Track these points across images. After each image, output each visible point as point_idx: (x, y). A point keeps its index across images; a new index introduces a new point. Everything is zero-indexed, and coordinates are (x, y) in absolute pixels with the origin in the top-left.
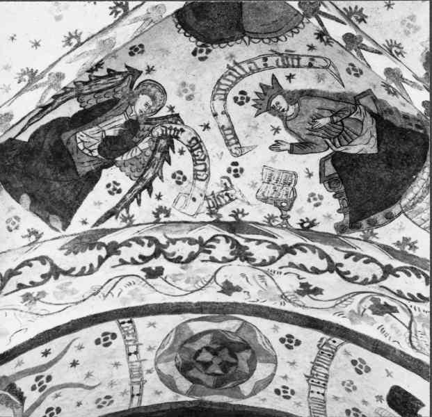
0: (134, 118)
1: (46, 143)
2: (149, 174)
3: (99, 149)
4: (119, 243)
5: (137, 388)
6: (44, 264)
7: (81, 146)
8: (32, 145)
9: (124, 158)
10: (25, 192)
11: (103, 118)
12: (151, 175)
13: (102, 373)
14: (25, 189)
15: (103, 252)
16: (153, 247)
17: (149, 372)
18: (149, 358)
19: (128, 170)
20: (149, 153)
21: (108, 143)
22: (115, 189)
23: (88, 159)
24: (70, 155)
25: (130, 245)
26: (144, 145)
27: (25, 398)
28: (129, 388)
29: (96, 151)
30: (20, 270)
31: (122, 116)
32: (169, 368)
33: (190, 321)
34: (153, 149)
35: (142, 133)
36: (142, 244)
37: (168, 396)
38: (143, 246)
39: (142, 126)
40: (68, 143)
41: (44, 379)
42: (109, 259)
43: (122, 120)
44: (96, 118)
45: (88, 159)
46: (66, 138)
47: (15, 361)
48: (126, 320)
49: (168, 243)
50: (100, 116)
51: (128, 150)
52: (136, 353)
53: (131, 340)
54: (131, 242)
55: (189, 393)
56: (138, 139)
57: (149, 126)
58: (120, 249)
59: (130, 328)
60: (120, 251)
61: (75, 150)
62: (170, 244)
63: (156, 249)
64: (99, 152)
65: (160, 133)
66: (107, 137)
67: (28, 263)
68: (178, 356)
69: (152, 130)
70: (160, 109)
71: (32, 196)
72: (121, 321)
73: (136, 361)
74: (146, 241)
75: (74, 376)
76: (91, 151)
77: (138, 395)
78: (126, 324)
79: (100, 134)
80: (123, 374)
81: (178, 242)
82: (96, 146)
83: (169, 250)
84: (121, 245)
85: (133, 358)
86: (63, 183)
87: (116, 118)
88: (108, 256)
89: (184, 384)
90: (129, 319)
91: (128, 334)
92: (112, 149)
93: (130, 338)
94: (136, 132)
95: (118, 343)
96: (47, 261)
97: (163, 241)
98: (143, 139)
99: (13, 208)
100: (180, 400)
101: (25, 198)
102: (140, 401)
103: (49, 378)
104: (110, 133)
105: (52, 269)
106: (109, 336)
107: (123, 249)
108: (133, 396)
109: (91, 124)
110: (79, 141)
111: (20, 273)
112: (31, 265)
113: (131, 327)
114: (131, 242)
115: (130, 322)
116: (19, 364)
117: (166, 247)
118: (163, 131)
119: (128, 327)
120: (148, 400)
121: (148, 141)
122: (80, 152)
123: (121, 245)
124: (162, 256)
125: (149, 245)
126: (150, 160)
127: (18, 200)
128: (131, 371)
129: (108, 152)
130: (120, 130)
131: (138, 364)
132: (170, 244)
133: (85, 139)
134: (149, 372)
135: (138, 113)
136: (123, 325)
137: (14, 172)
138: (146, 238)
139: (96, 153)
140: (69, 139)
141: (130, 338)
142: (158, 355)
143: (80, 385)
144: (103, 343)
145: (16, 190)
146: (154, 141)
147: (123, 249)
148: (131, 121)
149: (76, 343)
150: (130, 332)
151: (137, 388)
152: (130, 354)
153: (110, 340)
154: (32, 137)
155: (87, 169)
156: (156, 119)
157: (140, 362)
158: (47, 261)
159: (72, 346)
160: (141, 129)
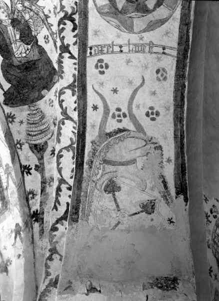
0: (10, 21)
1: (17, 75)
2: (41, 14)
3: (27, 44)
4: (61, 44)
5: (155, 49)
6: (64, 93)
7: (24, 55)
8: (15, 83)
9: (33, 30)
10: (41, 91)
11: (8, 40)
12: (43, 14)
13: (134, 74)
14: (39, 91)
15: (67, 55)
16: (66, 21)
17: (141, 39)
18: (125, 37)
19: (39, 29)
20: (32, 13)
21: (23, 39)
22: (152, 114)
23: (32, 52)
24: (28, 62)
25: (63, 37)
26: (27, 17)
27: (124, 128)
28: (154, 55)
29: (28, 46)
30: (64, 107)
31: (8, 28)
32: (139, 23)
33: (96, 5)
34: (30, 11)
35: (20, 17)
36: (63, 29)
37: (174, 25)
38: (65, 29)
39: (15, 17)
40: (20, 62)
41: (117, 113)
42: (71, 52)
43: (10, 29)
44: (6, 44)
45: (32, 52)
46: (18, 63)
47: (88, 129)
48: (89, 51)
49: (63, 11)
50: (6, 42)
51: (29, 27)
52: (121, 47)
53: (108, 50)
54: (61, 36)
55: (174, 9)
56: (23, 20)
57: (16, 12)
58: (65, 44)
59: (97, 49)
60: (67, 44)
61: (26, 59)
62: (64, 9)
63: (68, 20)
64: (29, 45)
65: (20, 5)
66: (20, 39)
67: (61, 102)
68: (129, 15)
69: (19, 11)
70: (6, 4)
71: (44, 88)
72: (88, 54)
73: (129, 47)
74: (62, 26)
75: (125, 93)
76: (28, 50)
77: (164, 49)
78: (93, 51)
79: (17, 43)
80: (138, 58)
81: (63, 4)
82: (26, 46)
83: (70, 11)
84: (63, 43)
85: (125, 49)
86: (43, 69)
87: (9, 32)
88: (70, 53)
89: (162, 12)
90: (89, 49)
91: (102, 50)
92: (27, 36)
93: (105, 49)
94: (18, 21)
95: (106, 58)
96: (63, 91)
97: (62, 15)
98: (23, 16)
99: (46, 101)
100: (179, 17)
101: (44, 92)
102: (171, 48)
103: (119, 110)
104: (18, 37)
105: (70, 88)
106: (99, 64)
107: (66, 42)
108: (164, 53)
109: (10, 48)
110: (20, 56)
111: (66, 108)
112: (63, 101)
113: (96, 48)
114: (61, 36)
115: (91, 48)
116: (93, 126)
117: (66, 14)
118: (19, 3)
119: (95, 51)
120: (173, 41)
121: (25, 13)
122: (27, 56)
123: (63, 43)
124: (74, 16)
125: (65, 24)
126: (35, 13)
127: (43, 97)
128: (136, 52)
129: (29, 40)
130: (17, 31)
131: (131, 46)
132: (64, 9)
133: (19, 52)
134: (141, 39)
135: (6, 18)
136: (93, 54)
137: (28, 96)
138: (59, 25)
139: (29, 47)
140: (19, 61)
141: (105, 49)
142: (125, 30)
143: (135, 92)
144: (104, 69)
145: (39, 96)
146: (25, 10)
147: (66, 42)
148: (11, 22)
149: (96, 87)
150: (100, 49)
151: (155, 49)
152: (121, 51)
153: (103, 64)
154: (9, 81)
155: (37, 54)
156: (12, 7)
157: (129, 44)
158: (63, 91)
159: (100, 91)
160: (17, 17)
